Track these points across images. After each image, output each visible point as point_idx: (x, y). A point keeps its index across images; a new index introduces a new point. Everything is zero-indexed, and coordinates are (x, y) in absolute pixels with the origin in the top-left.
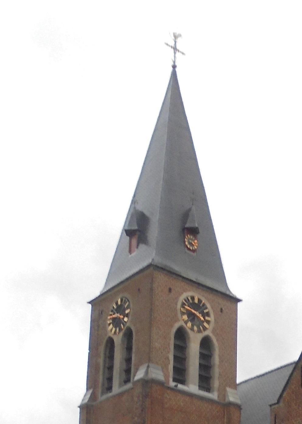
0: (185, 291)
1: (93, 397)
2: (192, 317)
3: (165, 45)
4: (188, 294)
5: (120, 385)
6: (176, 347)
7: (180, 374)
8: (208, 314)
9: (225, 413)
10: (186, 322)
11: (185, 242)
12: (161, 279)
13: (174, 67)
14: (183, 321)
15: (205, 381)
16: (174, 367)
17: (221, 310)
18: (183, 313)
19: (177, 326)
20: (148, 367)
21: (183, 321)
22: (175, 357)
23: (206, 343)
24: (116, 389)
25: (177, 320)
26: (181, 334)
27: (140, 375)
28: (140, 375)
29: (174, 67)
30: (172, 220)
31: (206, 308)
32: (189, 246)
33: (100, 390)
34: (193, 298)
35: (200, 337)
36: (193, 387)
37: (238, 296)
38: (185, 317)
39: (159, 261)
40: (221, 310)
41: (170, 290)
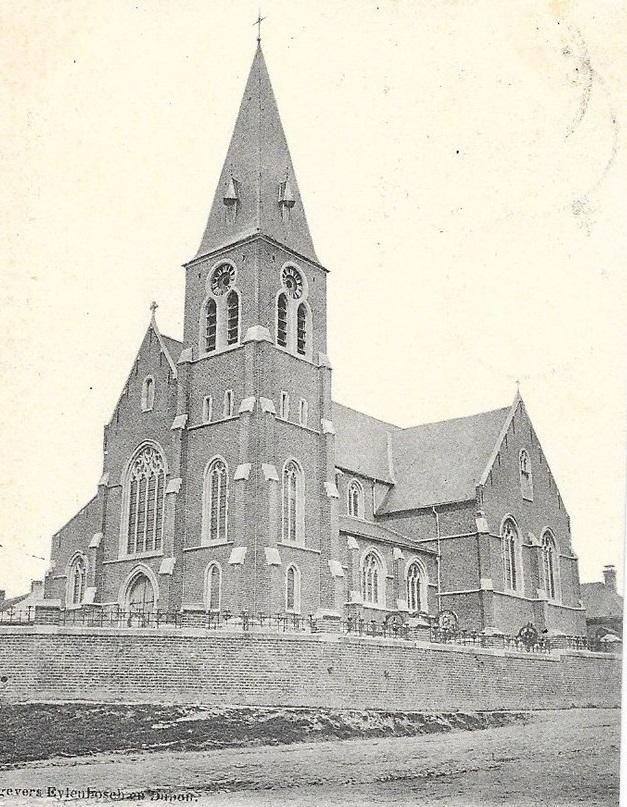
30: (257, 257)
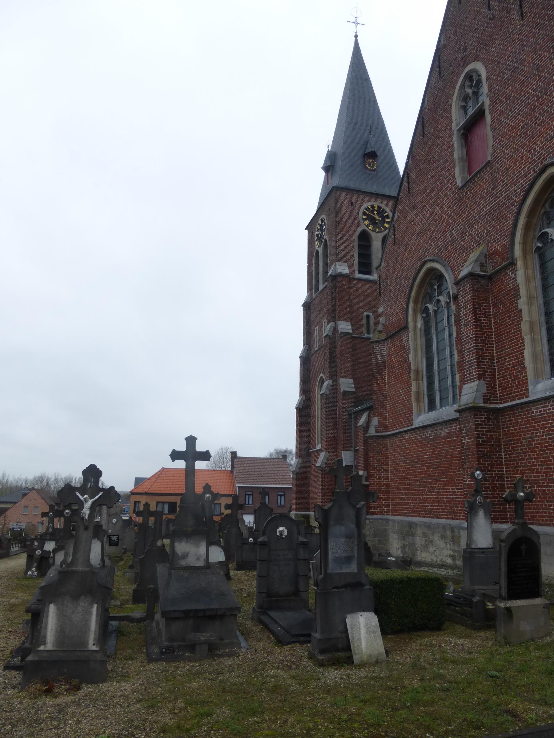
0: (365, 202)
2: (373, 221)
4: (368, 204)
6: (360, 246)
9: (314, 278)
10: (368, 226)
11: (365, 165)
12: (344, 197)
13: (356, 36)
14: (365, 225)
16: (359, 263)
18: (364, 220)
19: (359, 230)
20: (335, 265)
21: (365, 225)
22: (360, 255)
25: (360, 225)
26: (364, 237)
29: (356, 36)
31: (386, 212)
32: (369, 168)
33: (314, 291)
34: (373, 206)
35: (381, 235)
38: (367, 222)
39: (343, 184)
41: (352, 204)
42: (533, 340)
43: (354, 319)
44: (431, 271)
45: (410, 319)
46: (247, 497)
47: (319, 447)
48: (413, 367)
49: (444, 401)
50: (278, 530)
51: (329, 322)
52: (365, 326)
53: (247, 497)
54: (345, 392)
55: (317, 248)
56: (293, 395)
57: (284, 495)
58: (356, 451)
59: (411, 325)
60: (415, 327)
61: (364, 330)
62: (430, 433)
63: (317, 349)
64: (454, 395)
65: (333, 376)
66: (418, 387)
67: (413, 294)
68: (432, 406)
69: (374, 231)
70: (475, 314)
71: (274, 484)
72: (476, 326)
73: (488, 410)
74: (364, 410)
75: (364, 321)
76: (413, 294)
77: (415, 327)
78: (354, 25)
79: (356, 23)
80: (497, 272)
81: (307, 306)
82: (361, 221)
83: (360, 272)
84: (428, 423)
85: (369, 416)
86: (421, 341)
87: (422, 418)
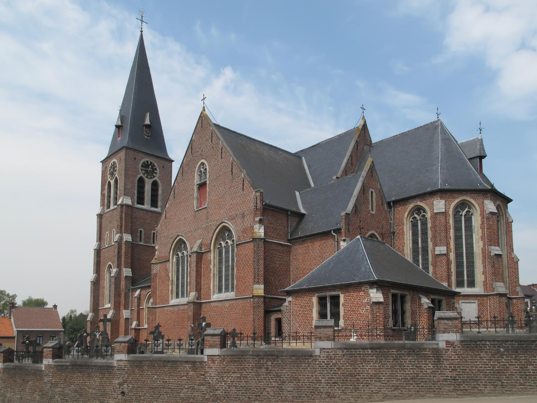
1: (103, 210)
3: (69, 311)
5: (114, 205)
6: (138, 186)
7: (141, 200)
8: (156, 169)
9: (106, 198)
13: (142, 31)
15: (154, 203)
17: (163, 167)
19: (139, 176)
22: (138, 192)
23: (155, 185)
24: (112, 207)
27: (119, 202)
28: (119, 202)
36: (147, 206)
37: (173, 159)
40: (163, 167)
41: (135, 159)
42: (214, 280)
43: (132, 233)
44: (181, 239)
45: (171, 257)
46: (38, 338)
47: (109, 306)
48: (171, 279)
49: (183, 296)
50: (339, 293)
51: (118, 233)
52: (139, 237)
53: (38, 338)
54: (126, 277)
55: (109, 180)
56: (89, 274)
57: (42, 336)
58: (132, 310)
59: (171, 260)
60: (173, 261)
61: (139, 239)
62: (176, 308)
63: (107, 246)
64: (187, 294)
65: (119, 266)
66: (172, 288)
67: (173, 247)
68: (177, 297)
69: (147, 177)
70: (196, 267)
71: (47, 328)
72: (196, 272)
73: (198, 303)
74: (138, 288)
75: (139, 234)
76: (173, 247)
77: (173, 261)
78: (140, 22)
79: (142, 21)
80: (205, 252)
81: (100, 216)
82: (140, 170)
83: (138, 203)
84: (176, 304)
85: (140, 291)
86: (175, 268)
87: (174, 301)
